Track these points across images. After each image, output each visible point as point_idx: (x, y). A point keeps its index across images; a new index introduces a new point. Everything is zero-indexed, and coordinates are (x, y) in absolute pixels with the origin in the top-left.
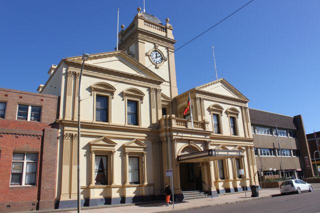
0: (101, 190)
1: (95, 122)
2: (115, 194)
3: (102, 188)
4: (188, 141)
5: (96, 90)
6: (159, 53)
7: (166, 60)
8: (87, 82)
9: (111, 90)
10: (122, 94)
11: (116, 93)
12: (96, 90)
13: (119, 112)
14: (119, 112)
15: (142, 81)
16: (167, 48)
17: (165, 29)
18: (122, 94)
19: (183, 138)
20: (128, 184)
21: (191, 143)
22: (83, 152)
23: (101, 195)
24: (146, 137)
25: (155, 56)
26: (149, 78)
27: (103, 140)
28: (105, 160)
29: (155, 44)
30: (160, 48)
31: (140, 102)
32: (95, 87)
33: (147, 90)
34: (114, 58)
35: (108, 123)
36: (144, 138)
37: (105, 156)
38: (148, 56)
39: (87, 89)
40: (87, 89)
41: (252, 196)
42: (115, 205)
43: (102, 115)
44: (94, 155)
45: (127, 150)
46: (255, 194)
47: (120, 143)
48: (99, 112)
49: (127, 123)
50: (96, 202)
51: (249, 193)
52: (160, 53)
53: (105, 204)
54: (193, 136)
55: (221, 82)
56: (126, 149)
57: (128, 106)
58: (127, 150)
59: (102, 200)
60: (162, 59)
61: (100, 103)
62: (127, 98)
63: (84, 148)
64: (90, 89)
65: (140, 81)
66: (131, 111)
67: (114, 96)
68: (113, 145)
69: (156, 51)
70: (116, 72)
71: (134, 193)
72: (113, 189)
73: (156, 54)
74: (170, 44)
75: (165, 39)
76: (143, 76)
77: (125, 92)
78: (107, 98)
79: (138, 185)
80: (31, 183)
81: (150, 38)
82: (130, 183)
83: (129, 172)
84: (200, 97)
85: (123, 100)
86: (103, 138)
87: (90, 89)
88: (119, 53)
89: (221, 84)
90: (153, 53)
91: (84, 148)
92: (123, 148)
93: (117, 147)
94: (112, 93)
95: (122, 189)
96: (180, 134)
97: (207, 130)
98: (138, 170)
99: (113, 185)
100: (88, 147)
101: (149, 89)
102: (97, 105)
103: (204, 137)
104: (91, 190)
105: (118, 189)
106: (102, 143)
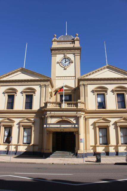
0: (104, 148)
1: (118, 109)
2: (112, 150)
3: (104, 146)
4: (61, 117)
5: (116, 91)
6: (68, 59)
7: (73, 62)
8: (91, 88)
9: (15, 91)
10: (113, 91)
11: (109, 91)
12: (116, 91)
13: (20, 103)
14: (20, 103)
15: (102, 81)
16: (74, 54)
17: (73, 42)
18: (113, 91)
19: (55, 115)
20: (120, 144)
21: (64, 118)
22: (91, 127)
23: (103, 150)
24: (35, 116)
25: (64, 61)
26: (42, 79)
27: (123, 119)
28: (105, 130)
29: (64, 54)
30: (68, 56)
31: (105, 94)
32: (95, 90)
33: (39, 87)
34: (19, 72)
35: (105, 110)
36: (33, 117)
37: (106, 128)
38: (59, 63)
39: (91, 92)
40: (91, 92)
41: (97, 161)
42: (111, 156)
43: (121, 105)
44: (119, 128)
45: (118, 124)
46: (98, 160)
47: (113, 121)
48: (120, 103)
49: (117, 107)
50: (112, 154)
51: (94, 159)
52: (69, 59)
53: (106, 155)
54: (64, 113)
55: (108, 68)
56: (118, 123)
57: (117, 97)
58: (118, 124)
59: (104, 153)
60: (70, 62)
61: (119, 98)
62: (116, 93)
63: (91, 125)
64: (93, 91)
65: (90, 81)
66: (121, 100)
67: (17, 95)
68: (13, 122)
69: (65, 58)
70: (97, 79)
71: (25, 149)
72: (110, 147)
73: (66, 60)
74: (76, 51)
75: (74, 49)
76: (37, 78)
77: (114, 89)
78: (104, 94)
79: (106, 145)
80: (104, 143)
81: (61, 51)
82: (122, 144)
83: (100, 137)
84: (45, 84)
85: (114, 94)
86: (123, 118)
87: (93, 91)
88: (21, 69)
89: (108, 70)
90: (63, 60)
91: (91, 125)
92: (115, 123)
93: (111, 123)
94: (106, 92)
95: (116, 147)
96: (53, 113)
97: (78, 108)
98: (29, 136)
99: (110, 145)
100: (94, 124)
101: (41, 86)
102: (117, 99)
103: (75, 113)
104: (119, 147)
105: (114, 147)
106: (26, 121)
